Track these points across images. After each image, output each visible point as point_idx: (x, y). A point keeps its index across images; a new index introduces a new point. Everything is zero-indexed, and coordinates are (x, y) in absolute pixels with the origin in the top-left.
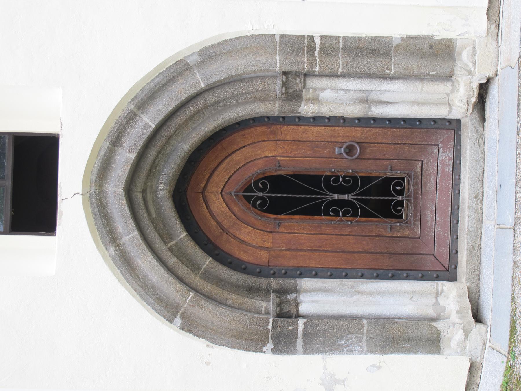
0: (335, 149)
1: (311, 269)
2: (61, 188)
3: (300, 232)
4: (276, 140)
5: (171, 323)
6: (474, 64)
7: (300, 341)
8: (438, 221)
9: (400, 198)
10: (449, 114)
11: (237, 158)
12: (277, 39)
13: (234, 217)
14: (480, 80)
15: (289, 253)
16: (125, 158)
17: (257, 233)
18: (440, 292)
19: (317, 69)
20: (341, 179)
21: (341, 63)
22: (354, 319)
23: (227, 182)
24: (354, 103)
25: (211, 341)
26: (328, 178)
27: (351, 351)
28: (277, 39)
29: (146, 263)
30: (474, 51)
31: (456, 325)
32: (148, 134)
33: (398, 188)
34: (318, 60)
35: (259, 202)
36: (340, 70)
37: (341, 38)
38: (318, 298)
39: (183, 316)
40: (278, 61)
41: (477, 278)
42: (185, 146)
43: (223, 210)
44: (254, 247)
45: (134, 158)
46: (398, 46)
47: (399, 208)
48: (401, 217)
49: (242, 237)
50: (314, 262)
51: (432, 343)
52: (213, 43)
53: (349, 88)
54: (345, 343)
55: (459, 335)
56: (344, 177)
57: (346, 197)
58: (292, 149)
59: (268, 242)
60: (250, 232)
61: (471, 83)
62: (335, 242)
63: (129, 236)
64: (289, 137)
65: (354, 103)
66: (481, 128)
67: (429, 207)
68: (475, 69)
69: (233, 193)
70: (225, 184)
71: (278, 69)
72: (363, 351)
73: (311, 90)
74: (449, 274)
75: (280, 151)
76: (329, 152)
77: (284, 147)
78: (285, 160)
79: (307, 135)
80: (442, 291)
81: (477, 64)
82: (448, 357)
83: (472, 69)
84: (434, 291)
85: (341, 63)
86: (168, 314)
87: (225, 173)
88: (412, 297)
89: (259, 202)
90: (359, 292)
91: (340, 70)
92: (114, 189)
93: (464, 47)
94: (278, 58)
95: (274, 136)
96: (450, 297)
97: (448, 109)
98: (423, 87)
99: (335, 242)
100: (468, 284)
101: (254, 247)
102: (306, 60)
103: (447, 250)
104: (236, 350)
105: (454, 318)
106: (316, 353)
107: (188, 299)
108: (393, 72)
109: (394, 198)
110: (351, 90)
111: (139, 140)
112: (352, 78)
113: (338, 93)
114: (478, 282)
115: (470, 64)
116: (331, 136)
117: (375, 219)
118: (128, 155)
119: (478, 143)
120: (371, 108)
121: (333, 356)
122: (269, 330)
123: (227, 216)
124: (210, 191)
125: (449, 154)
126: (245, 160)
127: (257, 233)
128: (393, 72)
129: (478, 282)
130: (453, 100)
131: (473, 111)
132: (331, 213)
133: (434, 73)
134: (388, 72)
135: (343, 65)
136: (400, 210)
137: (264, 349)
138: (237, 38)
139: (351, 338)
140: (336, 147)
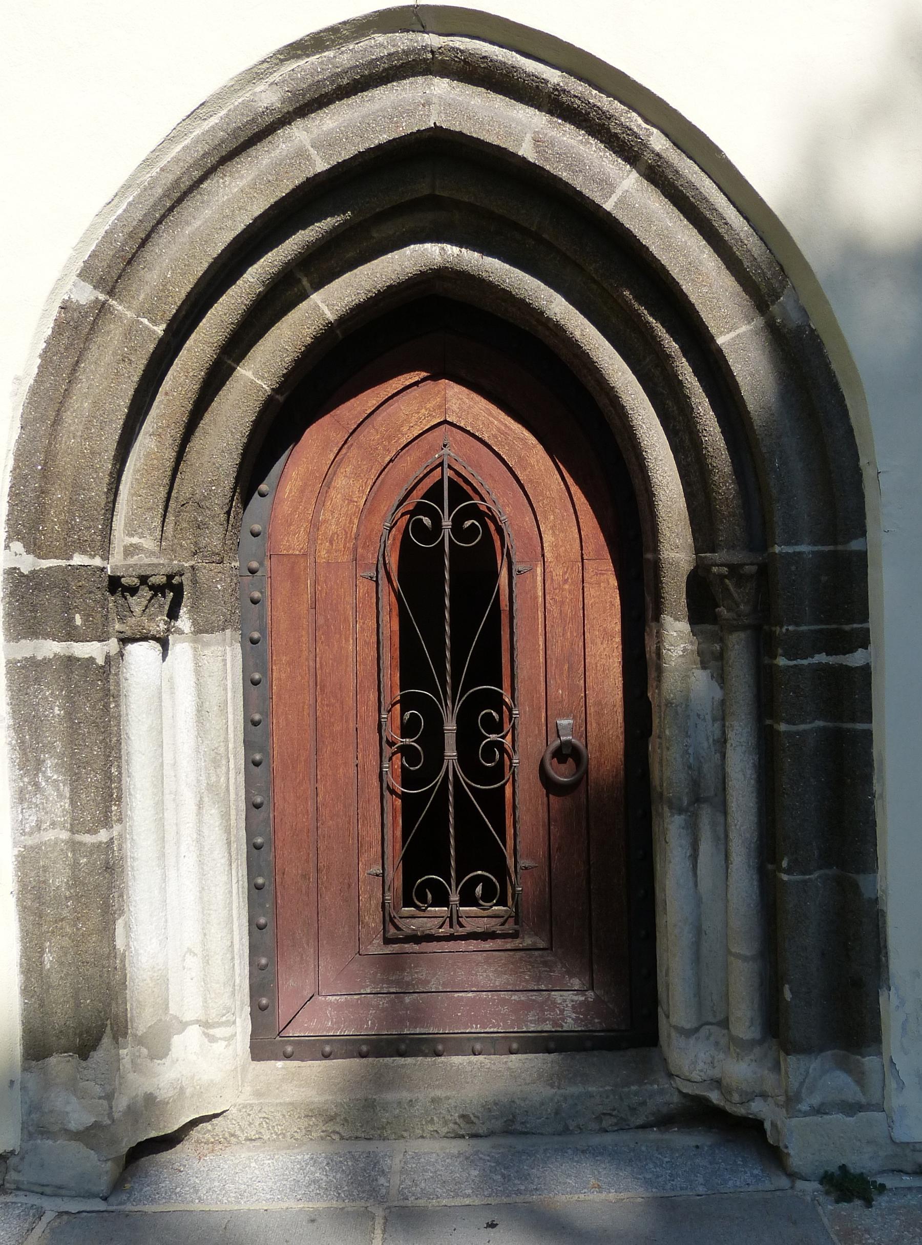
0: (568, 717)
1: (263, 667)
3: (360, 634)
4: (582, 559)
5: (79, 275)
6: (819, 1111)
7: (50, 648)
8: (402, 1002)
9: (454, 898)
10: (676, 1028)
11: (532, 461)
12: (855, 545)
13: (388, 459)
14: (774, 1125)
15: (303, 608)
17: (351, 522)
18: (211, 1031)
19: (782, 661)
20: (493, 737)
21: (802, 728)
23: (473, 435)
24: (690, 767)
25: (34, 391)
26: (496, 701)
27: (21, 800)
28: (855, 545)
30: (851, 1108)
31: (105, 1103)
32: (587, 192)
33: (479, 890)
34: (805, 662)
35: (427, 521)
36: (783, 727)
37: (864, 726)
39: (102, 308)
40: (798, 549)
41: (252, 1134)
43: (405, 429)
44: (316, 512)
45: (520, 154)
46: (855, 886)
47: (430, 896)
48: (408, 903)
49: (340, 482)
50: (283, 676)
52: (833, 366)
53: (730, 753)
54: (47, 779)
56: (500, 746)
57: (451, 752)
58: (563, 603)
59: (328, 552)
60: (351, 501)
61: (764, 1095)
62: (337, 728)
64: (591, 591)
65: (690, 767)
66: (640, 1121)
67: (435, 975)
68: (806, 1114)
69: (446, 450)
70: (468, 432)
71: (777, 549)
72: (23, 833)
73: (718, 647)
75: (557, 572)
76: (561, 702)
77: (566, 581)
78: (535, 587)
79: (599, 641)
80: (212, 1039)
81: (818, 1119)
82: (17, 1086)
83: (804, 1107)
84: (213, 1016)
85: (802, 727)
86: (101, 266)
87: (494, 431)
88: (195, 955)
89: (427, 521)
90: (200, 805)
91: (783, 727)
92: (435, 100)
93: (860, 1078)
94: (803, 548)
95: (592, 555)
97: (688, 1026)
98: (745, 959)
99: (337, 728)
100: (234, 1110)
101: (316, 512)
102: (803, 628)
103: (330, 1029)
104: (11, 463)
106: (12, 698)
107: (145, 321)
108: (785, 877)
109: (453, 883)
110: (723, 756)
111: (569, 167)
112: (756, 758)
113: (714, 720)
114: (243, 1137)
115: (816, 1100)
116: (600, 703)
117: (399, 833)
118: (528, 137)
119: (604, 1114)
120: (680, 814)
121: (8, 748)
122: (70, 558)
123: (389, 439)
124: (450, 393)
125: (569, 1020)
126: (531, 481)
127: (351, 522)
128: (785, 877)
129: (243, 1137)
131: (685, 1095)
132: (407, 715)
133: (788, 995)
134: (784, 864)
135: (797, 733)
136: (423, 900)
137: (18, 546)
138: (852, 430)
139: (61, 796)
140: (574, 718)
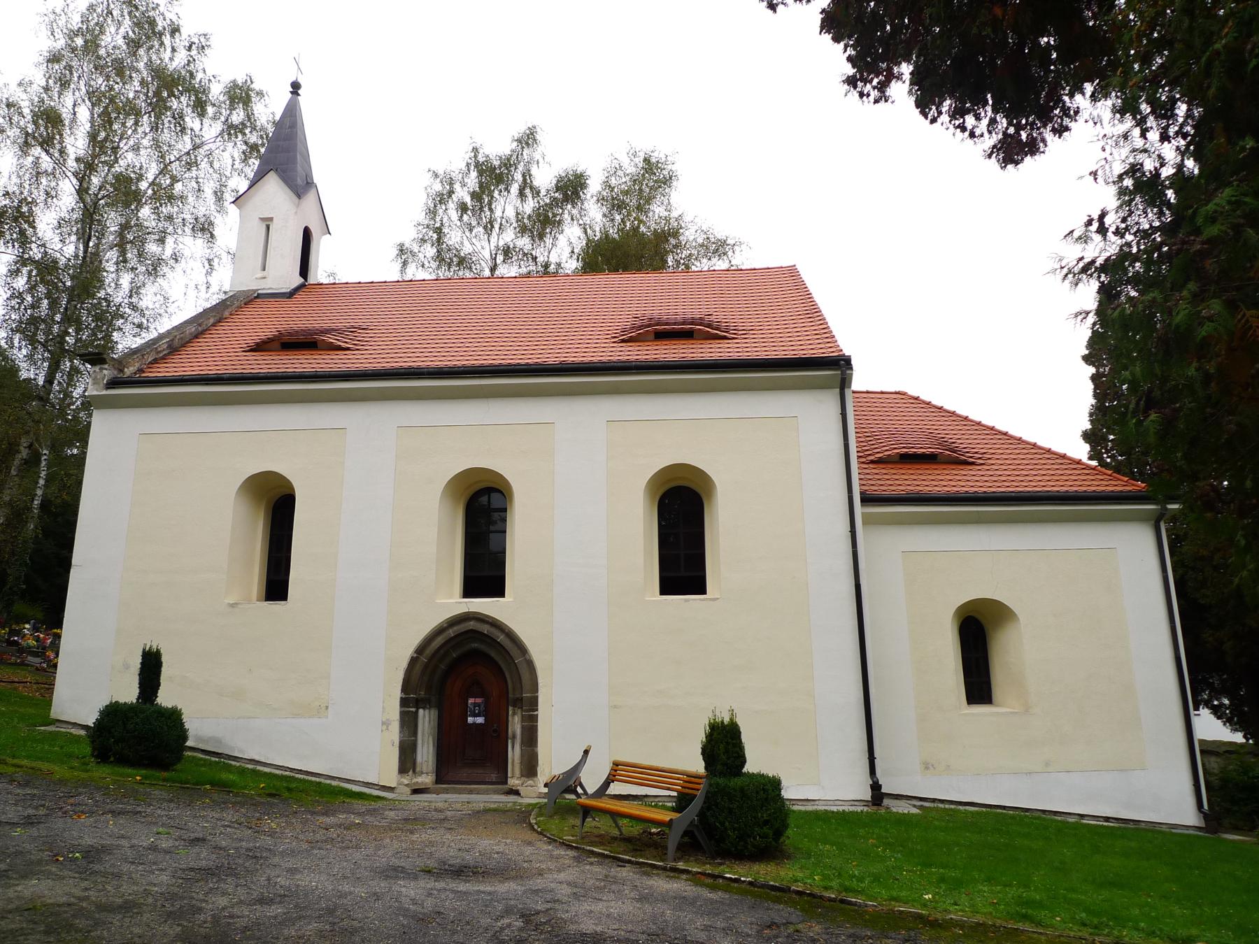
2: (686, 600)
16: (485, 629)
22: (415, 733)
29: (439, 641)
38: (426, 720)
42: (493, 654)
51: (403, 770)
55: (406, 782)
63: (451, 632)
74: (439, 780)
96: (426, 779)
105: (415, 780)
130: (513, 782)
